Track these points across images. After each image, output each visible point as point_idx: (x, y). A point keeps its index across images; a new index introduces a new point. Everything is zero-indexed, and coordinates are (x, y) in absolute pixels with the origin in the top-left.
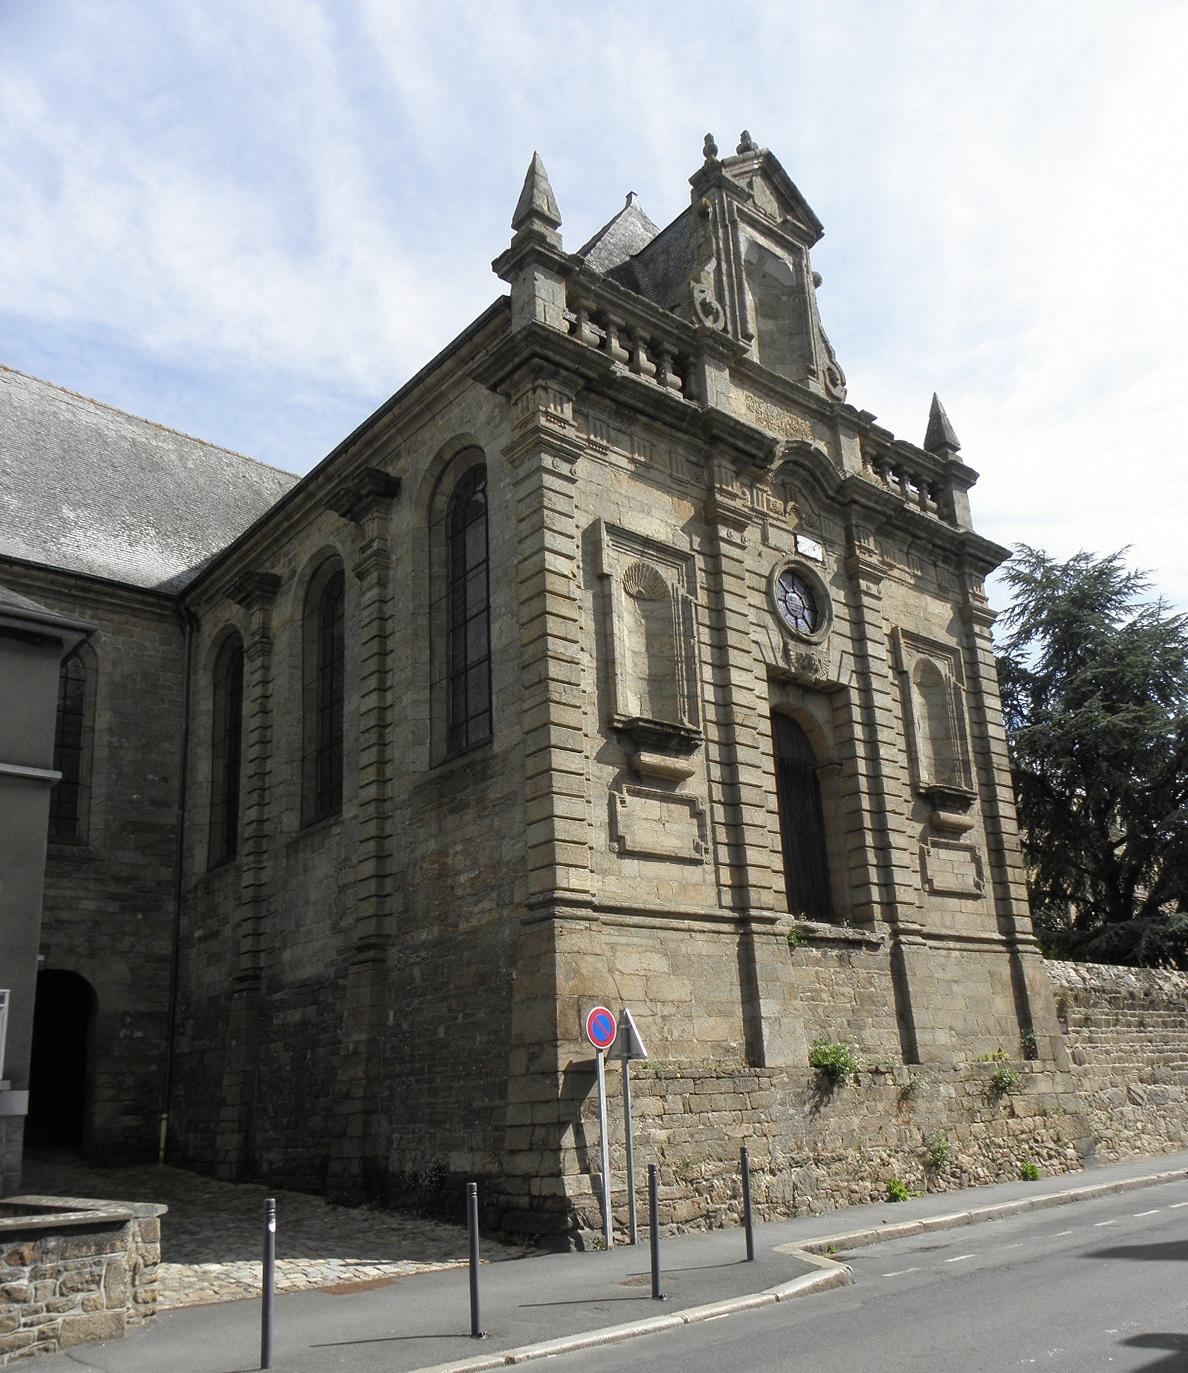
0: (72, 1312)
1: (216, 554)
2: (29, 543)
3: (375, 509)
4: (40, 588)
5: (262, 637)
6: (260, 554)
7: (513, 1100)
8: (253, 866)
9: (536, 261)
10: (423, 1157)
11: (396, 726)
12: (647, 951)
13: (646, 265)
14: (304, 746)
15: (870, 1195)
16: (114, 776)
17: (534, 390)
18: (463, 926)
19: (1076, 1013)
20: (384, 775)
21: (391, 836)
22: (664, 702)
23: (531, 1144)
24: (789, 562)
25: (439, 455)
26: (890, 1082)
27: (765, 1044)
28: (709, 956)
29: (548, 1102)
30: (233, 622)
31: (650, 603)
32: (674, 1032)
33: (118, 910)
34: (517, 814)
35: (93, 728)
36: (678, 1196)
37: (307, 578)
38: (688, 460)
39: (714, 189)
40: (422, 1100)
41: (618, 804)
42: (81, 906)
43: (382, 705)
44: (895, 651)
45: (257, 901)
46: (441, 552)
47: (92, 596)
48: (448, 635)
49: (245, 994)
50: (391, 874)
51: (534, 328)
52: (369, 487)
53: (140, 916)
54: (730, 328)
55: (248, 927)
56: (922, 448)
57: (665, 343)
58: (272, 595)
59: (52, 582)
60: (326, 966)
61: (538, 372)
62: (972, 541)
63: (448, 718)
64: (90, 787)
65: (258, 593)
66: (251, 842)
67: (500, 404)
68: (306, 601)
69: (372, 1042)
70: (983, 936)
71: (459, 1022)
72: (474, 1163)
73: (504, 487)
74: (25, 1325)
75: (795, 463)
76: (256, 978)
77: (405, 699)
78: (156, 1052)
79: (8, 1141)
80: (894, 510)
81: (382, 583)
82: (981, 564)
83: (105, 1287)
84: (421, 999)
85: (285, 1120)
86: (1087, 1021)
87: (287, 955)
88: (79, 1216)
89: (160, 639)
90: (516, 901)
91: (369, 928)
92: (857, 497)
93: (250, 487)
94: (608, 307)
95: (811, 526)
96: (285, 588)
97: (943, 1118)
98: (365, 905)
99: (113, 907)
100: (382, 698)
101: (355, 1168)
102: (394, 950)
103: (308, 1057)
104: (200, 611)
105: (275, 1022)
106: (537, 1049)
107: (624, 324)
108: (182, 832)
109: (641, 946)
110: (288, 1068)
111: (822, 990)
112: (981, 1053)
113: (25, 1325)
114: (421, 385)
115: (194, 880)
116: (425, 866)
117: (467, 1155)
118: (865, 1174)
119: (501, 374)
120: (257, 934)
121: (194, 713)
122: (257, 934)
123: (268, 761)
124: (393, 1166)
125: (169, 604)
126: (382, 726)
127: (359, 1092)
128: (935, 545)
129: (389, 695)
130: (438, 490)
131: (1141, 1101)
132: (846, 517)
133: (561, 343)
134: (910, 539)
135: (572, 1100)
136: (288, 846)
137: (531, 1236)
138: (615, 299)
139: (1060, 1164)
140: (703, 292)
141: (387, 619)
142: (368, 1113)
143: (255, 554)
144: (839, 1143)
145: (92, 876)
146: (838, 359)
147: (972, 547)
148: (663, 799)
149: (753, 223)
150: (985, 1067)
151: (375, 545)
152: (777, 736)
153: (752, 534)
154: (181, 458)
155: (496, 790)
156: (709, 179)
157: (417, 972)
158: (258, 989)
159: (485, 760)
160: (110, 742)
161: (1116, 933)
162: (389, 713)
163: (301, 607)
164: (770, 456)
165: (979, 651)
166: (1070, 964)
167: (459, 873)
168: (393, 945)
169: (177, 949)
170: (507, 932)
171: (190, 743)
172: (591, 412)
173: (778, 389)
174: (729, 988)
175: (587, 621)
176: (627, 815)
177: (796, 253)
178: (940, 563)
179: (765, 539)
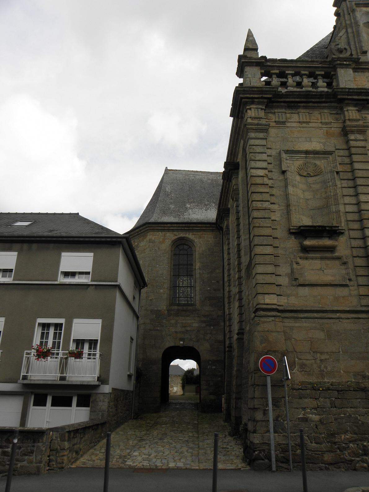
0: (24, 463)
2: (175, 217)
4: (176, 229)
16: (202, 283)
31: (315, 177)
33: (205, 326)
35: (195, 269)
38: (331, 114)
42: (193, 325)
47: (191, 228)
53: (212, 328)
57: (302, 72)
58: (228, 215)
59: (179, 227)
61: (246, 104)
64: (195, 287)
78: (220, 374)
79: (103, 401)
83: (35, 455)
89: (213, 237)
94: (284, 69)
99: (203, 325)
107: (293, 72)
109: (308, 327)
125: (214, 226)
135: (262, 398)
138: (286, 65)
145: (196, 315)
160: (200, 272)
172: (276, 111)
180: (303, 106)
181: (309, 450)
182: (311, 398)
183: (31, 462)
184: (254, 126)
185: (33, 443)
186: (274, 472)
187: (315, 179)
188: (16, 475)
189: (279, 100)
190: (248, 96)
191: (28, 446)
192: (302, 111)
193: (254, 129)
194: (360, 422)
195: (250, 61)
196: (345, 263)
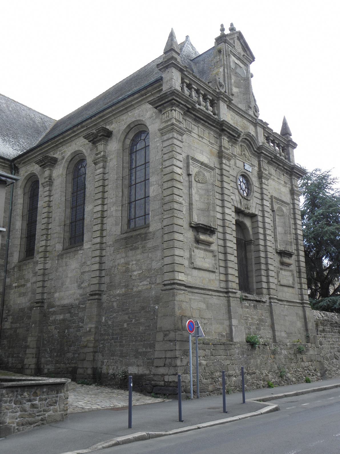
0: (50, 412)
1: (250, 213)
3: (103, 141)
5: (49, 179)
6: (49, 149)
7: (158, 349)
8: (43, 262)
9: (173, 67)
10: (117, 368)
11: (108, 218)
12: (200, 301)
13: (196, 64)
14: (65, 221)
15: (263, 386)
17: (171, 110)
18: (135, 289)
19: (321, 328)
20: (103, 234)
21: (105, 256)
22: (205, 218)
23: (165, 364)
24: (242, 172)
25: (129, 125)
26: (268, 349)
27: (233, 334)
28: (217, 304)
29: (172, 350)
30: (34, 172)
32: (207, 329)
34: (159, 253)
36: (209, 383)
37: (69, 160)
39: (223, 43)
40: (117, 349)
41: (192, 252)
43: (103, 210)
44: (272, 204)
45: (44, 275)
46: (127, 158)
48: (128, 188)
49: (39, 308)
50: (104, 270)
51: (175, 91)
52: (102, 133)
54: (227, 91)
55: (40, 284)
56: (280, 134)
57: (201, 91)
58: (53, 165)
60: (74, 300)
61: (173, 105)
62: (296, 168)
63: (128, 216)
65: (49, 163)
66: (42, 253)
67: (155, 112)
68: (67, 168)
69: (96, 328)
70: (294, 301)
71: (133, 322)
72: (139, 370)
73: (157, 141)
74: (38, 416)
75: (245, 139)
76: (43, 302)
77: (112, 209)
80: (274, 156)
81: (104, 167)
82: (298, 175)
84: (117, 313)
85: (55, 354)
86: (324, 331)
87: (57, 295)
88: (33, 382)
90: (158, 282)
91: (96, 288)
92: (263, 151)
93: (31, 119)
94: (192, 83)
95: (249, 160)
96: (59, 162)
97: (283, 361)
98: (94, 279)
100: (103, 208)
101: (90, 371)
102: (105, 296)
103: (66, 332)
104: (20, 166)
105: (51, 319)
106: (168, 332)
108: (8, 247)
110: (57, 336)
111: (249, 317)
112: (294, 340)
113: (38, 416)
114: (125, 101)
115: (13, 265)
116: (119, 268)
117: (136, 368)
118: (261, 379)
119: (160, 103)
120: (43, 287)
121: (15, 203)
122: (43, 287)
123: (50, 225)
124: (104, 371)
125: (8, 162)
126: (103, 217)
127: (91, 345)
128: (284, 168)
129: (106, 207)
130: (127, 137)
131: (338, 358)
132: (259, 157)
133: (182, 96)
134: (277, 166)
136: (58, 256)
137: (165, 395)
139: (316, 378)
140: (219, 78)
141: (105, 180)
142: (95, 352)
143: (47, 149)
144: (254, 368)
146: (257, 103)
147: (296, 170)
148: (205, 250)
149: (235, 55)
150: (295, 345)
151: (102, 153)
152: (237, 231)
153: (232, 162)
154: (7, 106)
155: (150, 244)
156: (221, 39)
157: (115, 304)
158: (43, 307)
159: (146, 233)
161: (329, 301)
162: (105, 213)
163: (66, 170)
164: (239, 136)
165: (296, 205)
166: (318, 311)
167: (135, 271)
168: (105, 294)
169: (4, 290)
170: (154, 292)
171: (12, 214)
172: (187, 119)
173: (240, 113)
174: (223, 315)
175: (185, 191)
176: (194, 255)
177: (247, 66)
178: (285, 174)
179: (235, 164)
180: (203, 123)
181: (203, 384)
182: (202, 350)
183: (55, 411)
184: (178, 128)
185: (57, 394)
186: (192, 399)
187: (201, 186)
188: (45, 424)
189: (192, 112)
190: (178, 99)
191: (53, 397)
192: (201, 126)
193: (177, 131)
194: (222, 365)
195: (177, 64)
196: (215, 256)
